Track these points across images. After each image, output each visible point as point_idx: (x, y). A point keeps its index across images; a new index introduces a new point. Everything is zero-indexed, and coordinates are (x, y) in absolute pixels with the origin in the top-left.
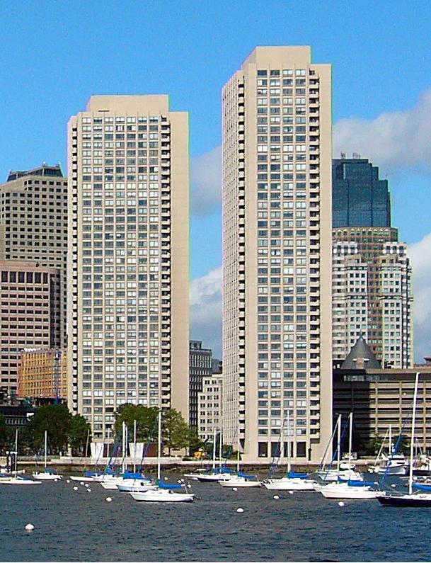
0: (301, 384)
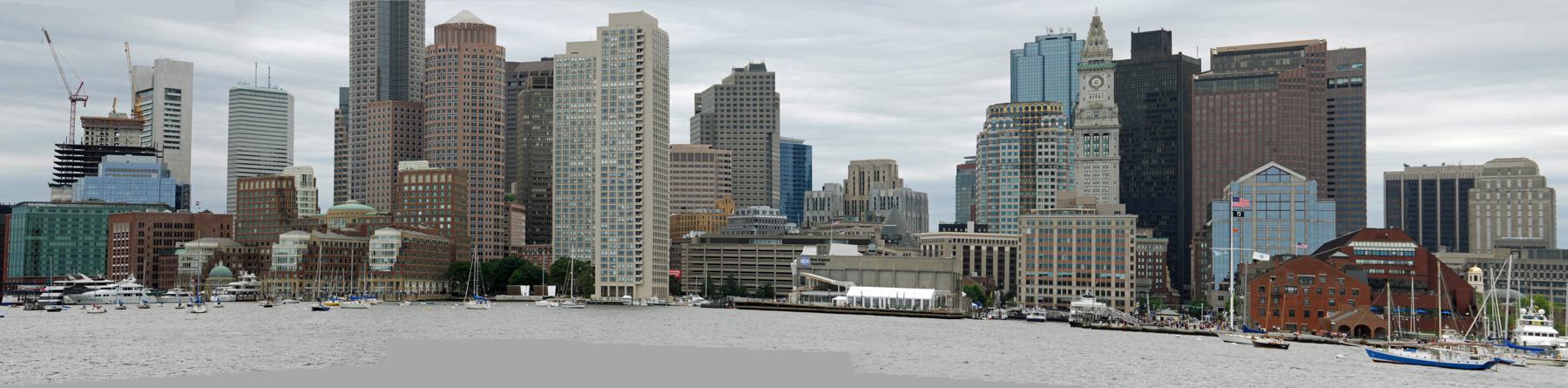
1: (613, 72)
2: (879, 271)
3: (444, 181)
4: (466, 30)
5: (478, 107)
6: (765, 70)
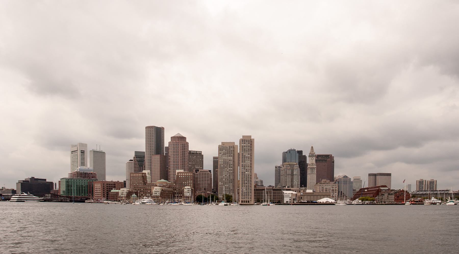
1: (245, 149)
2: (318, 195)
3: (186, 175)
4: (180, 138)
5: (184, 157)
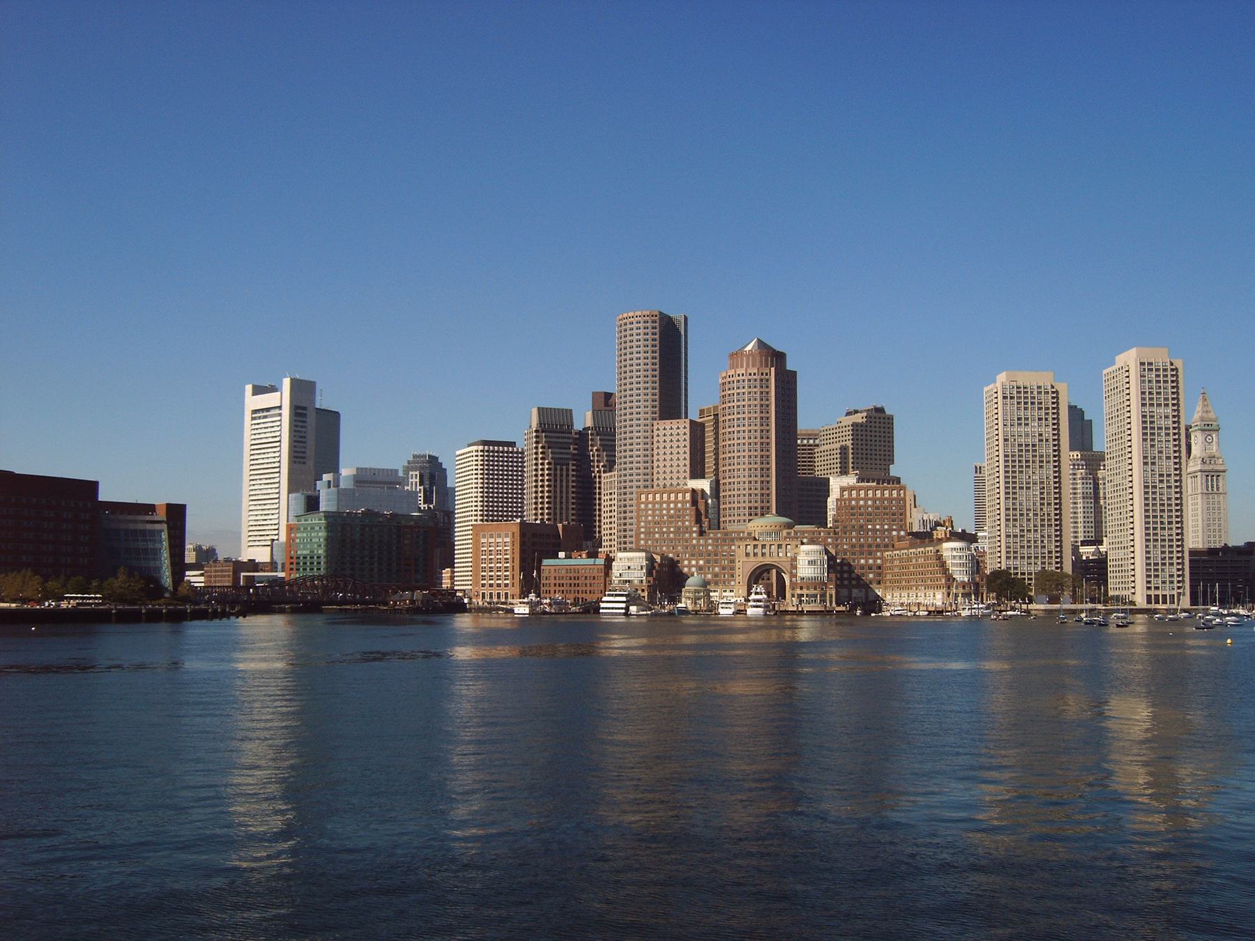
0: (1171, 558)
6: (885, 413)
